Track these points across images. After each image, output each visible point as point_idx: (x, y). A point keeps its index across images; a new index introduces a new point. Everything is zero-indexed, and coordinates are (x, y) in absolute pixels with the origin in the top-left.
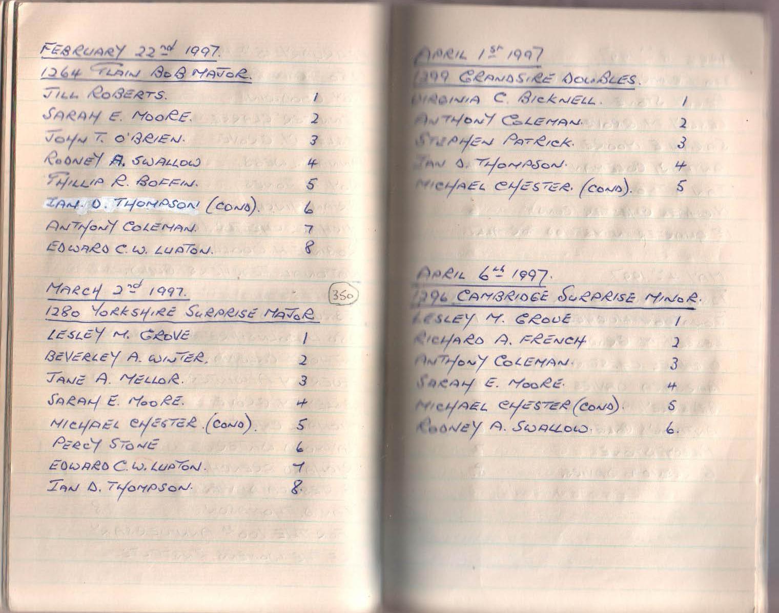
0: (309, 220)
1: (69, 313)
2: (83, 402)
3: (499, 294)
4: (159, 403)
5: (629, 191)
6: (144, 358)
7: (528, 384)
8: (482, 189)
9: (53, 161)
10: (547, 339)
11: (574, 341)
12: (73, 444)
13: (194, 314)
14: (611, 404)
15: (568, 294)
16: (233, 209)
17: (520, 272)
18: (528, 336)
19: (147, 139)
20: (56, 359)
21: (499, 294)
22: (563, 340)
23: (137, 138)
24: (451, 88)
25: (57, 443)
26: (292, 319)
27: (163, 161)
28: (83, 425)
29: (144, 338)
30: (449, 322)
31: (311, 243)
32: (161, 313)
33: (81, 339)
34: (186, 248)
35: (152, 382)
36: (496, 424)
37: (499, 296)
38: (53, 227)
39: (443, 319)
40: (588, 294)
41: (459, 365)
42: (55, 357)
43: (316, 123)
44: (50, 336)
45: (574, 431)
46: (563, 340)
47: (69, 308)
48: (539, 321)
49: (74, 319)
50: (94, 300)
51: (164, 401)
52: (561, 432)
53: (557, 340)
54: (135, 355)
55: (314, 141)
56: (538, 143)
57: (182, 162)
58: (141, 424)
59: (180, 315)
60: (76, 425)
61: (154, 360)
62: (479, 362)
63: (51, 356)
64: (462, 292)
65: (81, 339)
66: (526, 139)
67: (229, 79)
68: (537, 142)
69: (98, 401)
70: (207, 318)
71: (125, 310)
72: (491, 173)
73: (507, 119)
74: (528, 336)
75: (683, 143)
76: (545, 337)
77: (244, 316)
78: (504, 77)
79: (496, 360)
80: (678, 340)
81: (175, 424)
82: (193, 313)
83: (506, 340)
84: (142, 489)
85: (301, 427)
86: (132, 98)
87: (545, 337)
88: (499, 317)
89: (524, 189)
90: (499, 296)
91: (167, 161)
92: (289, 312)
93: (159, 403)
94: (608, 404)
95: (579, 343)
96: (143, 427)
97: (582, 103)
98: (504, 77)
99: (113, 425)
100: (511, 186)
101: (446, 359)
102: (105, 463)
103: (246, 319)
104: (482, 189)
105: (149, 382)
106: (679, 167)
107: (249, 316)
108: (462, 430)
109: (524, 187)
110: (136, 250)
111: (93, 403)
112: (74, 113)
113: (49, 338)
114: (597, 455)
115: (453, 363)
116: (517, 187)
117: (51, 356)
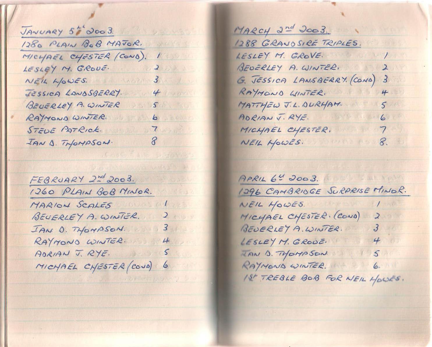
1: (37, 45)
3: (47, 179)
6: (290, 242)
9: (33, 119)
14: (138, 55)
15: (333, 189)
16: (56, 119)
17: (259, 30)
21: (47, 179)
23: (100, 192)
24: (245, 185)
25: (64, 129)
27: (39, 253)
28: (78, 57)
29: (305, 27)
30: (59, 46)
37: (47, 180)
39: (258, 242)
40: (349, 190)
41: (269, 268)
44: (295, 80)
48: (303, 57)
50: (267, 57)
54: (293, 67)
55: (166, 228)
56: (80, 131)
58: (296, 217)
61: (309, 230)
62: (257, 266)
64: (269, 189)
66: (74, 129)
67: (393, 194)
68: (79, 130)
73: (290, 216)
75: (386, 80)
78: (62, 118)
80: (151, 262)
81: (110, 241)
84: (299, 255)
91: (95, 206)
96: (297, 218)
98: (62, 118)
102: (44, 253)
105: (262, 243)
110: (275, 106)
113: (294, 82)
114: (168, 120)
115: (243, 105)
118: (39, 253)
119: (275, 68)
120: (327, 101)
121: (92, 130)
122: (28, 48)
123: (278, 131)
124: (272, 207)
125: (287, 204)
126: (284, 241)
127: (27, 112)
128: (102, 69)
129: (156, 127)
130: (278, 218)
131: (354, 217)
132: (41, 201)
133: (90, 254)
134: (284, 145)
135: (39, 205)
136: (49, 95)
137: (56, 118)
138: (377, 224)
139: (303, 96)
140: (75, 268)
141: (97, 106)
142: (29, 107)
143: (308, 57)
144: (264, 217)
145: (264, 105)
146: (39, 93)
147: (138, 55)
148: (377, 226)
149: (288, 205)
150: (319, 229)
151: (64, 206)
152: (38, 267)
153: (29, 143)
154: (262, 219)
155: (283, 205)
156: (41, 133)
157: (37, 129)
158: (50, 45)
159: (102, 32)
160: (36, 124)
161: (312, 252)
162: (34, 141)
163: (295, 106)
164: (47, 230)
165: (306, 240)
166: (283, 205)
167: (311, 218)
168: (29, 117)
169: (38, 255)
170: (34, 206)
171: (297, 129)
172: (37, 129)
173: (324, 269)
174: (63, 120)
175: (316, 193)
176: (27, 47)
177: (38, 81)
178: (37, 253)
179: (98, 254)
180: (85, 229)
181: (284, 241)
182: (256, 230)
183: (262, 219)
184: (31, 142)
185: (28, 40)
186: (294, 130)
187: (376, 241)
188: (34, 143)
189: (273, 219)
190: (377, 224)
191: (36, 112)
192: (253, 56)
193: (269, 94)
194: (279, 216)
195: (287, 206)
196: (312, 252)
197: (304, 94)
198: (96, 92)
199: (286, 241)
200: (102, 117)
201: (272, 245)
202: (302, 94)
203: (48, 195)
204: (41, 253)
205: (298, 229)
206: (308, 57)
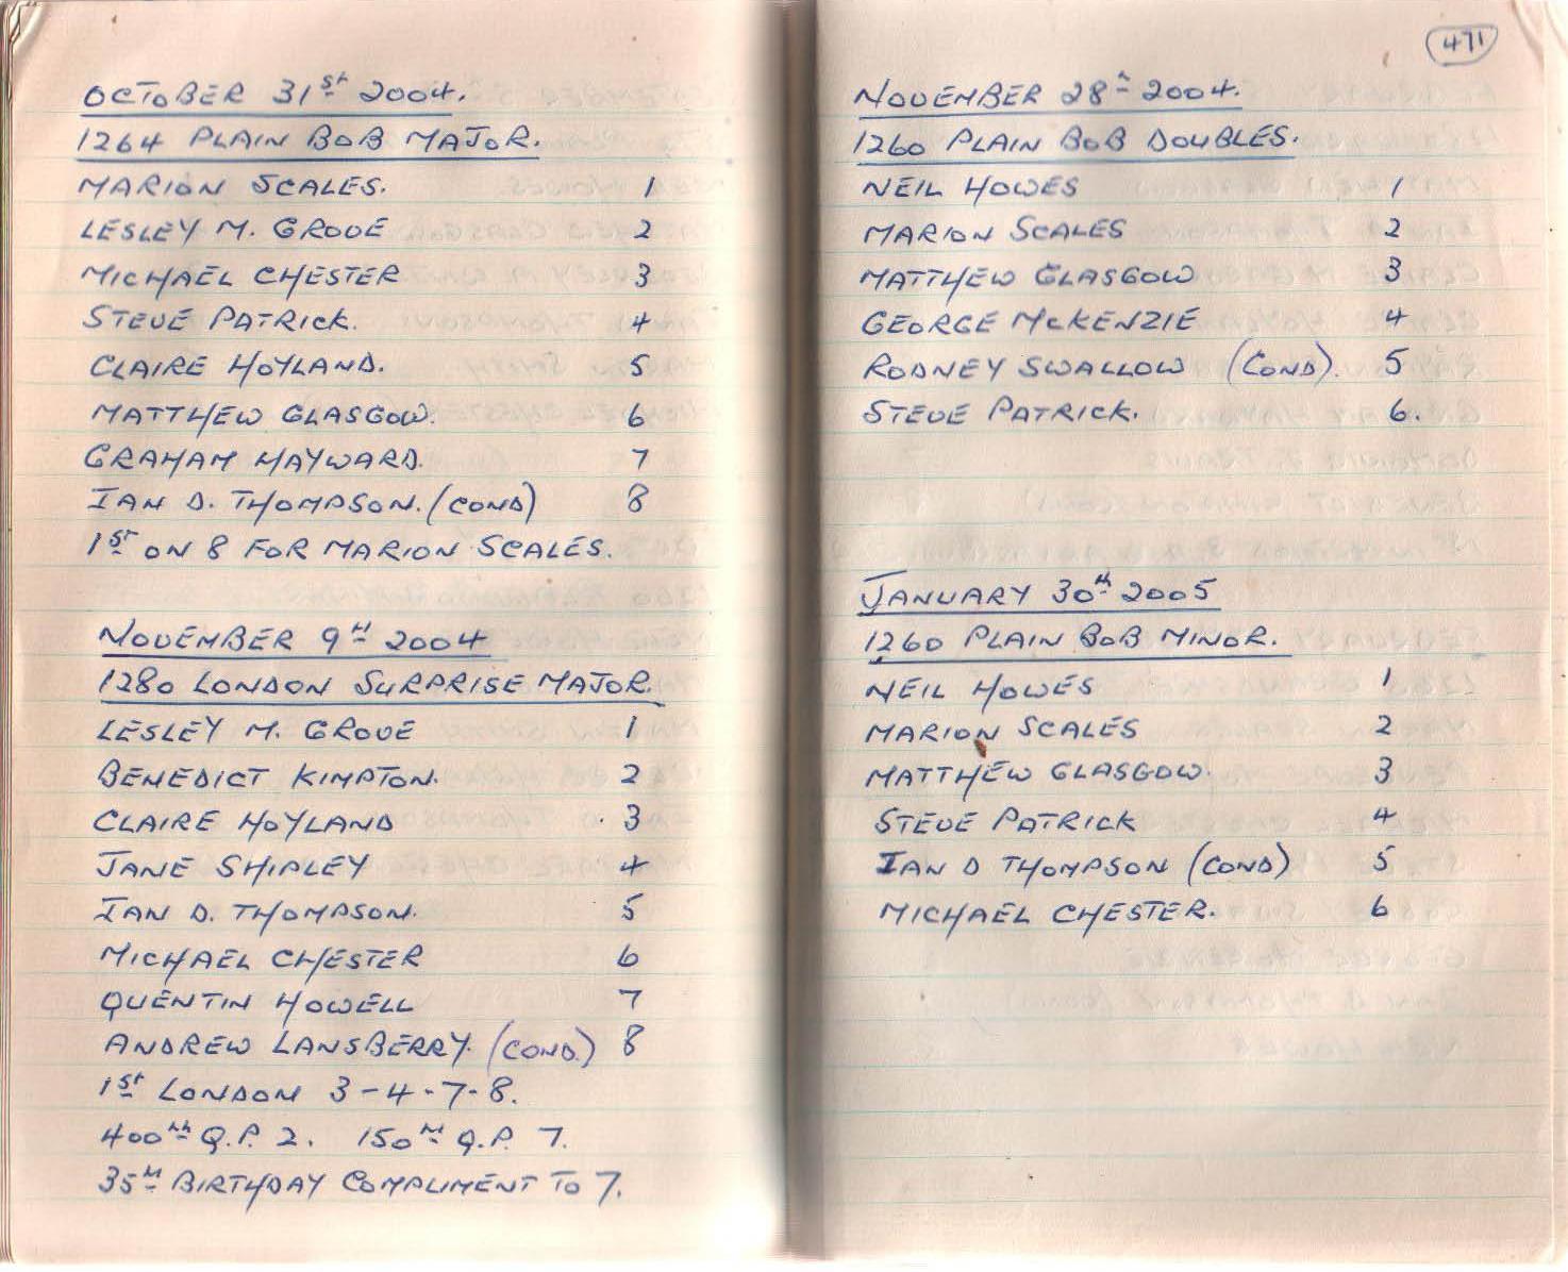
4: (926, 329)
7: (1046, 229)
12: (1027, 92)
13: (374, 689)
15: (375, 679)
18: (260, 541)
19: (635, 685)
20: (123, 783)
21: (1131, 633)
25: (1103, 106)
29: (379, 90)
31: (222, 540)
33: (303, 374)
35: (1116, 372)
37: (1132, 635)
38: (122, 190)
42: (120, 776)
49: (1081, 606)
51: (936, 325)
52: (287, 1052)
59: (342, 690)
60: (972, 321)
62: (308, 1185)
63: (111, 772)
65: (303, 374)
72: (202, 434)
74: (260, 541)
77: (495, 689)
80: (428, 522)
88: (270, 728)
90: (1132, 635)
92: (595, 680)
93: (926, 329)
94: (512, 498)
96: (950, 922)
99: (380, 1005)
100: (285, 276)
101: (248, 498)
103: (501, 695)
107: (506, 689)
109: (974, 281)
111: (197, 418)
116: (266, 505)
117: (111, 772)
119: (264, 641)
120: (188, 541)
121: (290, 183)
124: (285, 1008)
125: (1026, 187)
126: (883, 230)
128: (252, 643)
133: (284, 323)
136: (223, 782)
139: (1030, 152)
140: (1022, 917)
143: (937, 644)
144: (251, 365)
145: (201, 417)
146: (127, 229)
149: (1030, 188)
150: (139, 1046)
154: (245, 370)
155: (1020, 690)
158: (884, 912)
161: (125, 826)
163: (225, 280)
164: (150, 912)
166: (1020, 690)
167: (116, 1082)
168: (301, 772)
171: (955, 276)
173: (1207, 917)
174: (506, 509)
176: (96, 148)
179: (355, 868)
181: (883, 230)
182: (94, 102)
183: (245, 370)
186: (1081, 916)
187: (1393, 319)
192: (140, 232)
195: (1025, 194)
196: (125, 826)
197: (868, 187)
199: (270, 728)
200: (387, 824)
201: (530, 514)
202: (1027, 145)
203: (154, 695)
205: (1072, 730)
206: (937, 644)
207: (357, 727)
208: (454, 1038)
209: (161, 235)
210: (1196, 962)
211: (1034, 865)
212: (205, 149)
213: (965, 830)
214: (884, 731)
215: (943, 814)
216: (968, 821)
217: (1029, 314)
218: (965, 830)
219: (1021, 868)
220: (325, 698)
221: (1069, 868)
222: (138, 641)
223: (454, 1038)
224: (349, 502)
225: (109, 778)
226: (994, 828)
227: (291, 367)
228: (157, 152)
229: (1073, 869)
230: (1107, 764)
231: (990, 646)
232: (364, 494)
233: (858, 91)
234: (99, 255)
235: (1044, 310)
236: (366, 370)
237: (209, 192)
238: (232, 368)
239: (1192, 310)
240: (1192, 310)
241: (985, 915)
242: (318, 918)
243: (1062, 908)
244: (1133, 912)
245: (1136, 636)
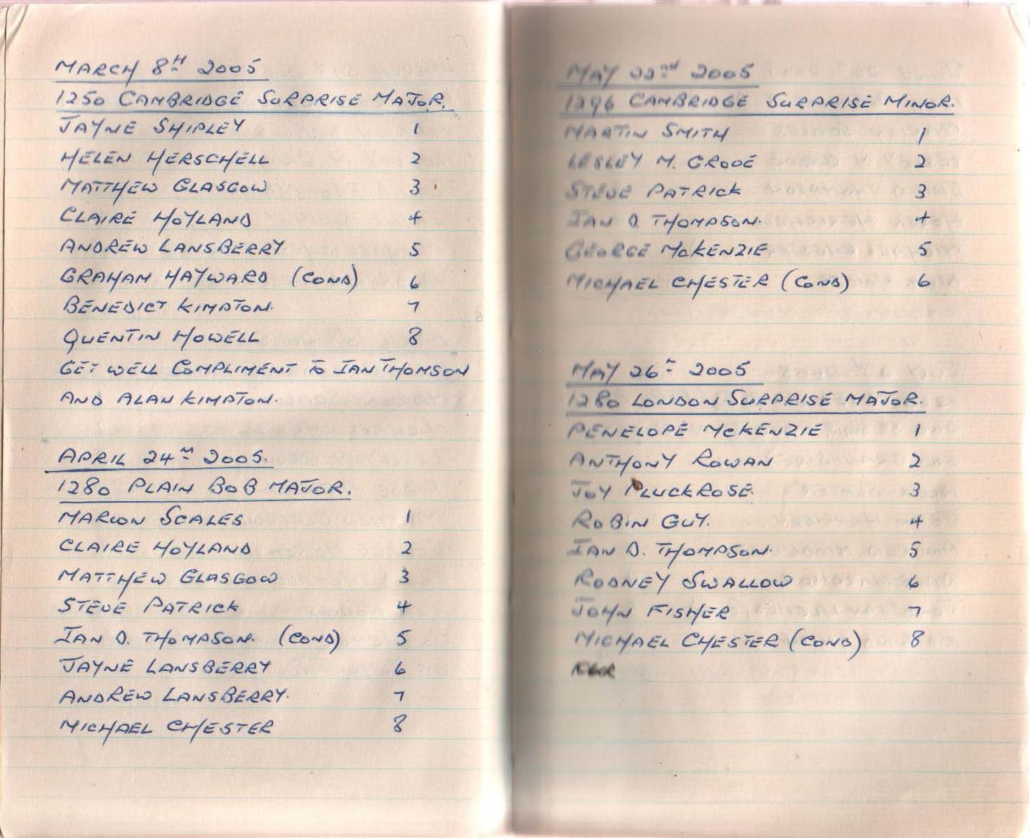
0: (414, 296)
2: (86, 70)
5: (126, 642)
8: (253, 341)
10: (749, 161)
11: (219, 160)
22: (209, 607)
26: (310, 495)
27: (70, 244)
30: (99, 162)
32: (833, 104)
34: (238, 398)
36: (68, 695)
37: (250, 486)
43: (75, 493)
45: (176, 523)
46: (209, 607)
47: (233, 490)
49: (103, 498)
53: (119, 158)
57: (646, 401)
69: (134, 69)
70: (798, 110)
71: (701, 248)
76: (126, 692)
79: (694, 577)
82: (770, 582)
83: (73, 456)
85: (414, 253)
86: (97, 731)
87: (126, 692)
89: (353, 104)
90: (250, 486)
95: (113, 282)
96: (112, 282)
97: (239, 340)
104: (253, 341)
105: (245, 341)
106: (921, 221)
108: (237, 162)
111: (164, 219)
112: (103, 66)
118: (70, 244)
122: (70, 104)
123: (239, 340)
126: (72, 516)
127: (65, 261)
129: (403, 693)
130: (646, 286)
131: (710, 103)
132: (85, 509)
134: (730, 467)
135: (80, 517)
136: (714, 193)
137: (130, 520)
138: (916, 484)
141: (199, 100)
142: (68, 310)
147: (836, 280)
148: (917, 487)
151: (329, 282)
152: (66, 186)
153: (65, 638)
156: (91, 613)
157: (84, 602)
159: (723, 372)
160: (77, 288)
162: (75, 633)
165: (836, 99)
169: (66, 250)
170: (68, 519)
172: (84, 602)
175: (862, 106)
177: (88, 157)
178: (64, 396)
180: (405, 368)
184: (68, 637)
185: (68, 88)
188: (76, 639)
189: (649, 645)
190: (916, 484)
191: (82, 262)
193: (935, 105)
194: (649, 283)
198: (221, 481)
200: (246, 550)
203: (160, 464)
204: (74, 245)
207: (713, 490)
208: (665, 457)
209: (101, 340)
210: (301, 557)
211: (709, 640)
212: (139, 493)
213: (120, 613)
214: (72, 516)
215: (105, 603)
216: (759, 642)
217: (185, 488)
218: (120, 613)
219: (114, 190)
220: (191, 496)
221: (698, 222)
222: (102, 492)
223: (665, 457)
224: (211, 637)
225: (71, 308)
226: (129, 491)
227: (196, 549)
228: (170, 464)
229: (700, 222)
230: (753, 460)
231: (147, 491)
232: (738, 638)
233: (848, 395)
234: (111, 160)
235: (723, 425)
236: (98, 702)
237: (584, 636)
238: (705, 517)
239: (214, 724)
240: (214, 724)
241: (631, 285)
242: (211, 311)
243: (178, 363)
244: (732, 642)
245: (253, 486)
